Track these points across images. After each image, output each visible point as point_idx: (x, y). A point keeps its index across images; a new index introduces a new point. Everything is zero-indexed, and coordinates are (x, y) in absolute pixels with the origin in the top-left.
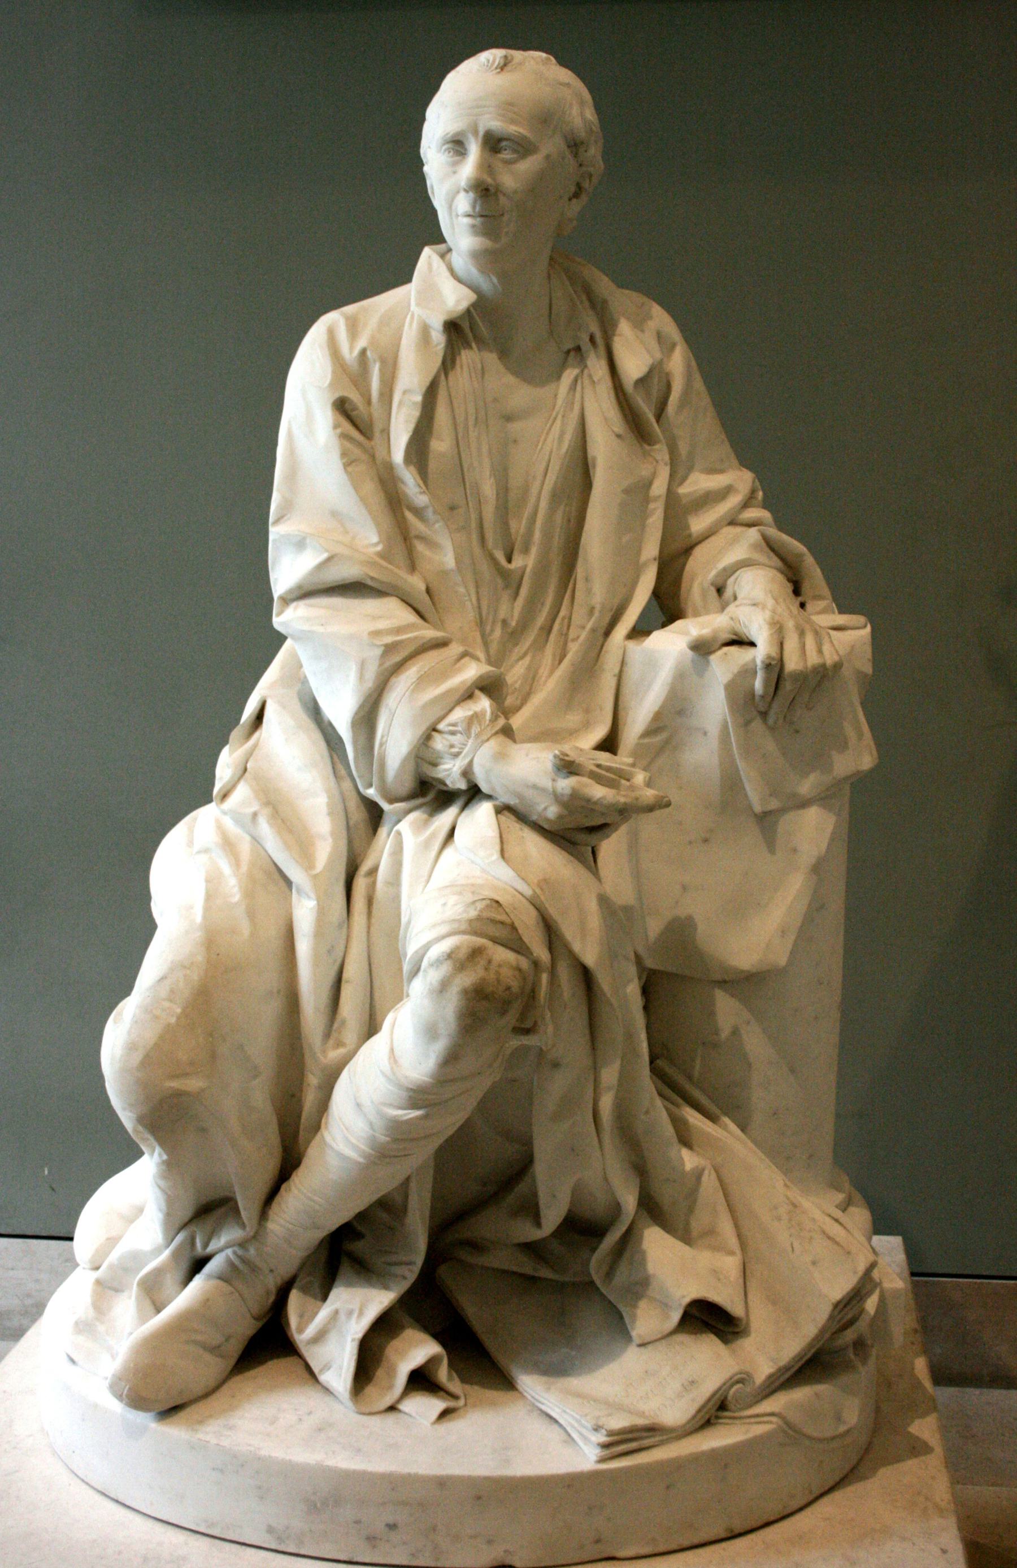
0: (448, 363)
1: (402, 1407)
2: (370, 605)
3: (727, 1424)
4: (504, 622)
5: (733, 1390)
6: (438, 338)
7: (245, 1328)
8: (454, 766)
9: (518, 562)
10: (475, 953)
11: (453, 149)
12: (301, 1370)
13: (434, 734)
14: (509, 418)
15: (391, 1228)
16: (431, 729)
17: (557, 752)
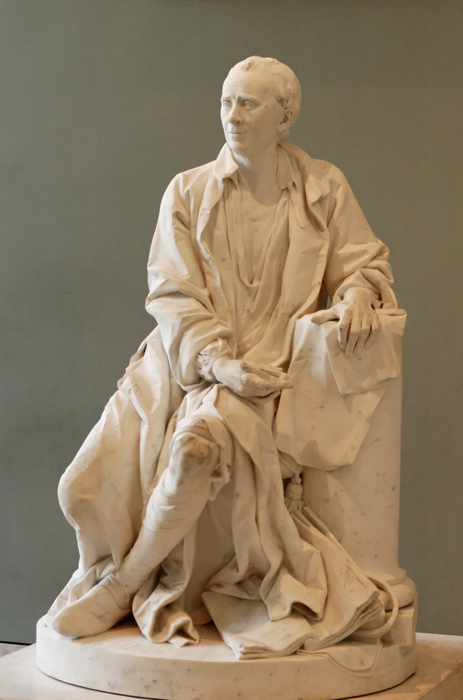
0: (225, 196)
1: (172, 641)
2: (181, 301)
3: (304, 655)
4: (248, 311)
5: (308, 640)
6: (221, 185)
7: (117, 613)
8: (206, 369)
9: (255, 284)
10: (191, 439)
11: (227, 104)
12: (139, 632)
13: (199, 356)
14: (254, 220)
15: (178, 571)
16: (198, 353)
17: (242, 363)
